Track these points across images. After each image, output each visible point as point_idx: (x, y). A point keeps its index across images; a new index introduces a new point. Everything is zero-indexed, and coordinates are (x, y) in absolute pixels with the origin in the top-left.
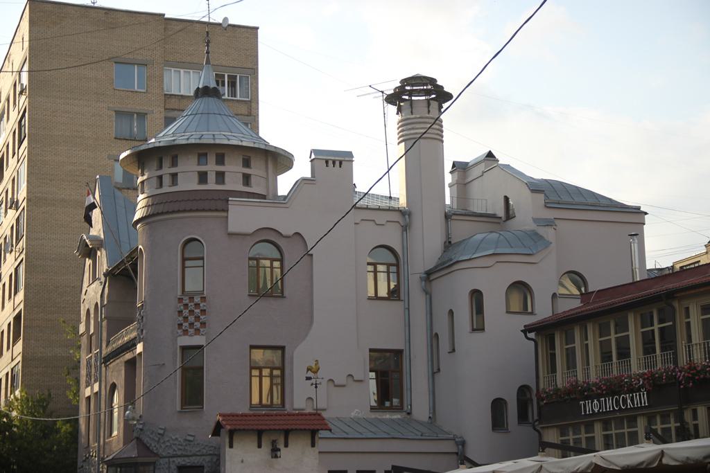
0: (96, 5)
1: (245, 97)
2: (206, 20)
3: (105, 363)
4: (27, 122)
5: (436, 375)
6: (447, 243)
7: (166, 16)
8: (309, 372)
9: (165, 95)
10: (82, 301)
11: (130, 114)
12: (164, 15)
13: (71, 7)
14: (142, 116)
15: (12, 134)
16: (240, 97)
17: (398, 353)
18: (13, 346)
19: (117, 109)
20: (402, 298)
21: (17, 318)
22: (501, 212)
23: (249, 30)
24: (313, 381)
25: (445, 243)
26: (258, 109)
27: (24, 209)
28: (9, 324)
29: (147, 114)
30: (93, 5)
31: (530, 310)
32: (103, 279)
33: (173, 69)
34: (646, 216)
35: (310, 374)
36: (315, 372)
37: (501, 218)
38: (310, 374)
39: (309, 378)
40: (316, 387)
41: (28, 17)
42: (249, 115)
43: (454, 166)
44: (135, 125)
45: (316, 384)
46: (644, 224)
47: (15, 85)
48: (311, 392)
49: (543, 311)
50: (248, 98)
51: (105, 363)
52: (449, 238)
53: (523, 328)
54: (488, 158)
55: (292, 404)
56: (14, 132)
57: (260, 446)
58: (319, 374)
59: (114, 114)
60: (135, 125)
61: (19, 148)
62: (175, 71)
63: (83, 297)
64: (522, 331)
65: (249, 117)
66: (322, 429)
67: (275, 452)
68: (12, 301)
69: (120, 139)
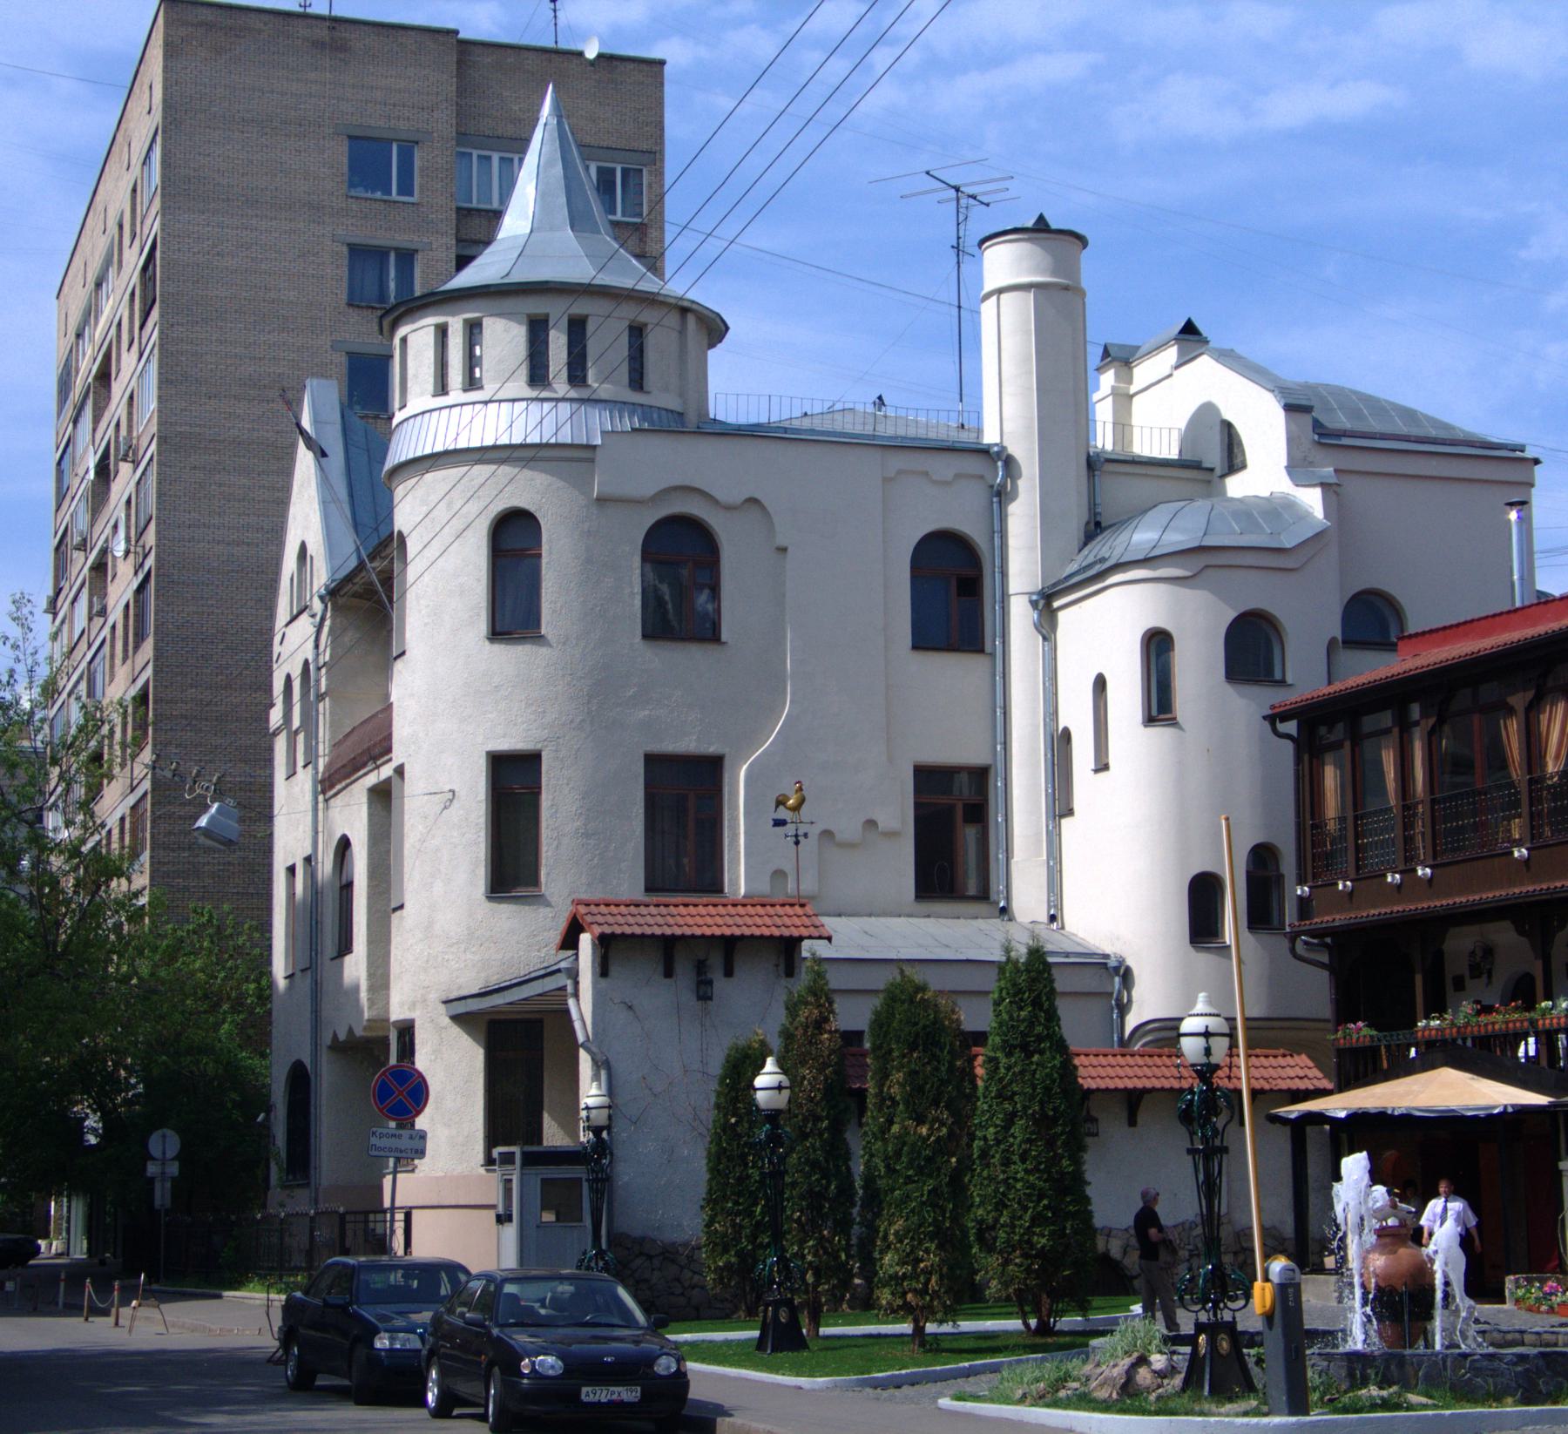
0: (309, 10)
1: (634, 216)
3: (324, 792)
4: (158, 269)
6: (1092, 526)
7: (461, 36)
8: (781, 807)
10: (275, 658)
12: (456, 32)
13: (252, 15)
15: (127, 296)
16: (624, 214)
17: (981, 775)
20: (988, 648)
23: (644, 67)
25: (1088, 523)
29: (417, 251)
30: (302, 10)
31: (1278, 676)
32: (317, 606)
33: (475, 153)
34: (1537, 468)
35: (783, 813)
37: (1212, 470)
39: (779, 823)
40: (797, 843)
41: (161, 42)
46: (1532, 485)
48: (783, 854)
51: (324, 792)
52: (1096, 514)
53: (1270, 712)
54: (1182, 336)
55: (1122, 426)
56: (133, 294)
59: (345, 250)
61: (142, 327)
63: (276, 648)
64: (1265, 718)
66: (810, 937)
67: (704, 991)
68: (129, 767)
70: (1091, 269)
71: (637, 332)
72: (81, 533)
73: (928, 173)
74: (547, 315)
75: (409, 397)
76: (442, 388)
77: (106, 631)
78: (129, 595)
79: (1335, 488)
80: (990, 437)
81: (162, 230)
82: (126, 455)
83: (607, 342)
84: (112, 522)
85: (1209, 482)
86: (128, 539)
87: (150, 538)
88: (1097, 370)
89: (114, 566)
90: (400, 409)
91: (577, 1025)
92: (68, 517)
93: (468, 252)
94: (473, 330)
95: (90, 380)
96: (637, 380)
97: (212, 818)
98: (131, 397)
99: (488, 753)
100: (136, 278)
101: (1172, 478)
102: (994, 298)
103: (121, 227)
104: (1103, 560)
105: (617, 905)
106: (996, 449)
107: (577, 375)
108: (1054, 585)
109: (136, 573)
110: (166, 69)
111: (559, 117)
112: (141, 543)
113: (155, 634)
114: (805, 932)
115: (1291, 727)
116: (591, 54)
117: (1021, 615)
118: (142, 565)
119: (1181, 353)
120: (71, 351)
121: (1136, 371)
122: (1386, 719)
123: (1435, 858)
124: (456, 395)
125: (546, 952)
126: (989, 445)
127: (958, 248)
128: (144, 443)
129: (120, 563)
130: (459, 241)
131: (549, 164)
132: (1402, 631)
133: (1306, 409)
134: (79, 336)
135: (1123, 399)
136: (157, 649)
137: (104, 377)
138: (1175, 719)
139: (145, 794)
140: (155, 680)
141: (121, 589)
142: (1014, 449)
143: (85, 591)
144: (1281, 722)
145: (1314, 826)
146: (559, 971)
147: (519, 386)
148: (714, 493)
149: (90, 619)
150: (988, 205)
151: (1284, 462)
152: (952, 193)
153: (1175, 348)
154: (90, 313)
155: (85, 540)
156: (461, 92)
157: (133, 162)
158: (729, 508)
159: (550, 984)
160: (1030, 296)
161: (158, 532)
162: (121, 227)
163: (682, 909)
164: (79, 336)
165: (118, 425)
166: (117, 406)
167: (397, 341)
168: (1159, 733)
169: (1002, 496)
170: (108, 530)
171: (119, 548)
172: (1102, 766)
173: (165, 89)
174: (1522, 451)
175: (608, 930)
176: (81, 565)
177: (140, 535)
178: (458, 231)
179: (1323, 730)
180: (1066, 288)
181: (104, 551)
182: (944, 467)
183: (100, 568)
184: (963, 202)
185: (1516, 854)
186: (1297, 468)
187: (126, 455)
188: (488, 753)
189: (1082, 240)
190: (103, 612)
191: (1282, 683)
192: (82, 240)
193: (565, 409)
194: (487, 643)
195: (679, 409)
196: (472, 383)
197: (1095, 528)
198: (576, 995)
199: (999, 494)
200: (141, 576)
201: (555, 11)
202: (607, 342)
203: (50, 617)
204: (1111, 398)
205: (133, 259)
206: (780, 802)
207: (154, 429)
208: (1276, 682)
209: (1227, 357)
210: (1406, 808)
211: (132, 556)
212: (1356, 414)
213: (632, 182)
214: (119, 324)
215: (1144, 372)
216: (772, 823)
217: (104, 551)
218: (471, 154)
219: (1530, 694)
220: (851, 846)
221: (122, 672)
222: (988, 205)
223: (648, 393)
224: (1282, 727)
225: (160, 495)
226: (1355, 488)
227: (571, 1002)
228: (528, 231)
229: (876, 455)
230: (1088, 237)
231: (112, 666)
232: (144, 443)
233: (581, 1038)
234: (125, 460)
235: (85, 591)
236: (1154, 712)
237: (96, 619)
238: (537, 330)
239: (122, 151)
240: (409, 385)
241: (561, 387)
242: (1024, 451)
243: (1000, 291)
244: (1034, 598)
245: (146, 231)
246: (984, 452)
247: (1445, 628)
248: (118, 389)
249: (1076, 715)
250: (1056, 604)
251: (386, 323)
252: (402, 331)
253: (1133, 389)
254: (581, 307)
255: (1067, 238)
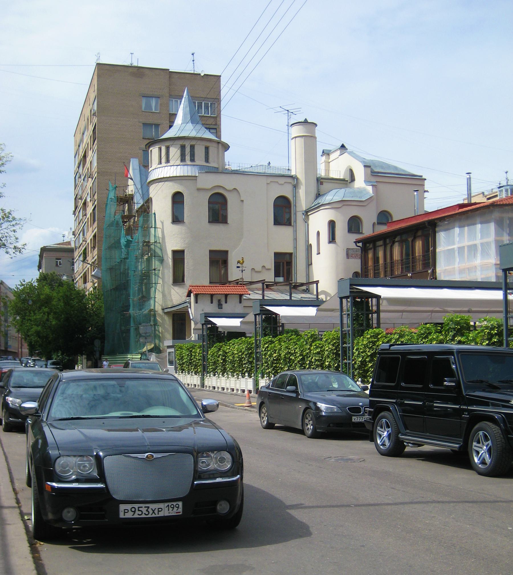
2: (192, 72)
5: (310, 266)
6: (318, 195)
9: (170, 114)
11: (151, 125)
12: (169, 70)
14: (157, 126)
17: (291, 254)
18: (93, 251)
19: (143, 122)
21: (95, 236)
22: (348, 178)
23: (216, 77)
24: (241, 269)
25: (317, 194)
26: (221, 121)
27: (96, 177)
28: (91, 239)
29: (159, 125)
33: (174, 100)
35: (239, 265)
36: (242, 264)
37: (347, 181)
38: (239, 265)
39: (238, 267)
40: (242, 272)
42: (216, 125)
43: (323, 152)
44: (154, 131)
45: (242, 270)
47: (91, 111)
49: (367, 231)
50: (209, 114)
52: (319, 192)
53: (355, 241)
54: (341, 148)
55: (327, 170)
56: (91, 136)
57: (212, 303)
58: (244, 265)
59: (142, 125)
60: (154, 131)
61: (93, 145)
62: (175, 101)
64: (354, 242)
65: (216, 126)
69: (145, 139)
70: (318, 132)
71: (207, 148)
72: (80, 195)
73: (280, 107)
74: (185, 144)
75: (152, 165)
76: (160, 163)
77: (86, 219)
78: (91, 211)
79: (375, 186)
80: (293, 173)
81: (97, 121)
82: (90, 176)
83: (200, 152)
84: (87, 193)
85: (347, 184)
86: (91, 197)
87: (96, 197)
88: (321, 156)
89: (88, 203)
90: (151, 167)
91: (191, 315)
92: (77, 191)
93: (171, 125)
94: (168, 148)
95: (82, 157)
96: (207, 160)
97: (95, 273)
98: (91, 162)
99: (172, 250)
100: (91, 133)
101: (337, 183)
102: (294, 139)
103: (88, 120)
104: (319, 203)
105: (200, 287)
106: (294, 176)
107: (192, 160)
108: (308, 209)
109: (93, 205)
110: (98, 81)
111: (188, 95)
112: (94, 198)
113: (97, 221)
114: (244, 293)
115: (360, 244)
116: (202, 75)
117: (300, 217)
118: (94, 203)
119: (340, 152)
120: (77, 150)
121: (330, 156)
122: (380, 243)
123: (391, 276)
124: (164, 164)
125: (184, 298)
126: (293, 175)
127: (288, 125)
128: (94, 173)
129: (89, 203)
130: (170, 122)
131: (186, 107)
132: (392, 220)
133: (369, 167)
134: (79, 146)
135: (328, 163)
136: (98, 224)
137: (85, 157)
138: (335, 242)
139: (96, 260)
140: (97, 232)
141: (90, 209)
142: (298, 176)
143: (82, 209)
144: (358, 243)
145: (365, 268)
146: (186, 302)
147: (178, 162)
148: (225, 187)
149: (83, 216)
150: (296, 114)
151: (364, 180)
152: (287, 112)
153: (339, 151)
154: (82, 140)
155: (81, 197)
156: (170, 85)
157: (91, 103)
158: (229, 191)
159: (185, 305)
160: (302, 140)
161: (97, 196)
162: (88, 120)
163: (215, 288)
164: (79, 146)
165: (88, 169)
166: (88, 164)
167: (150, 151)
168: (332, 245)
169: (295, 187)
170: (86, 195)
171: (88, 200)
172: (319, 253)
173: (98, 86)
174: (422, 177)
175: (197, 293)
176: (80, 203)
177: (93, 196)
178: (170, 119)
179: (368, 245)
180: (312, 137)
181: (85, 200)
182: (282, 181)
183: (85, 204)
184: (289, 114)
185: (409, 275)
186: (366, 181)
187: (90, 176)
188: (172, 250)
189: (316, 125)
190: (86, 215)
191: (362, 233)
192: (79, 122)
193: (189, 167)
194: (171, 224)
195: (217, 167)
196: (168, 161)
197: (318, 195)
198: (190, 308)
199: (295, 187)
200: (94, 206)
201: (194, 63)
202: (200, 152)
203: (74, 215)
204: (324, 163)
205: (91, 128)
206: (238, 262)
207: (96, 170)
208: (361, 233)
209: (351, 153)
210: (392, 263)
211: (92, 201)
212: (382, 167)
213: (213, 106)
214: (88, 144)
215: (333, 156)
216: (287, 249)
217: (85, 200)
218: (173, 100)
219: (412, 238)
220: (259, 272)
221: (90, 229)
222: (296, 114)
223: (210, 163)
224: (358, 244)
225: (98, 186)
226: (381, 186)
227: (189, 309)
228: (181, 124)
229: (265, 178)
230: (317, 124)
231: (88, 228)
232: (94, 173)
233: (191, 318)
234: (90, 178)
235: (82, 209)
236: (331, 240)
237: (84, 216)
238: (183, 148)
239: (88, 100)
240: (152, 162)
241: (188, 162)
242: (301, 177)
243: (296, 137)
244: (303, 212)
245: (94, 121)
246: (291, 177)
247: (398, 221)
248: (88, 159)
249: (313, 240)
250: (309, 214)
251: (147, 147)
252: (151, 149)
253: (330, 161)
254: (193, 143)
255: (314, 125)
